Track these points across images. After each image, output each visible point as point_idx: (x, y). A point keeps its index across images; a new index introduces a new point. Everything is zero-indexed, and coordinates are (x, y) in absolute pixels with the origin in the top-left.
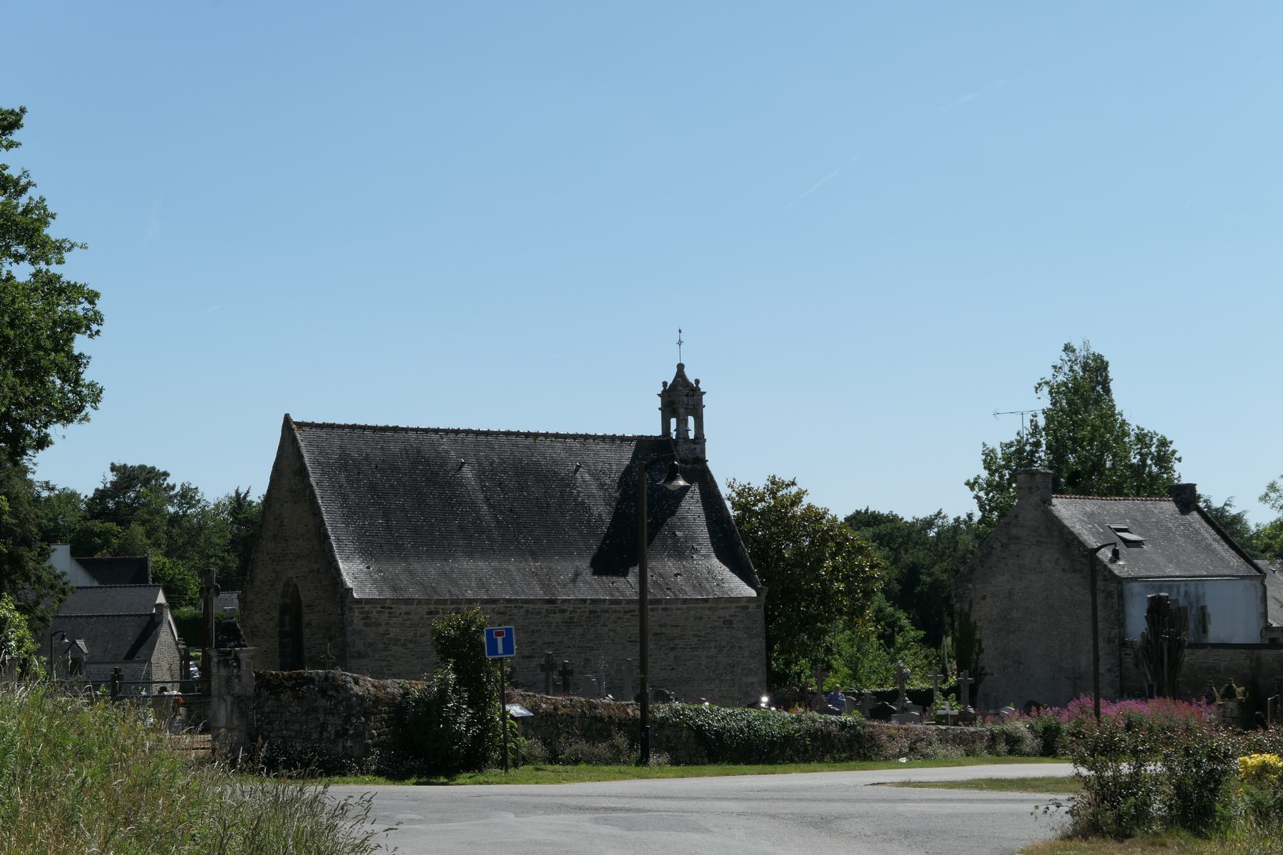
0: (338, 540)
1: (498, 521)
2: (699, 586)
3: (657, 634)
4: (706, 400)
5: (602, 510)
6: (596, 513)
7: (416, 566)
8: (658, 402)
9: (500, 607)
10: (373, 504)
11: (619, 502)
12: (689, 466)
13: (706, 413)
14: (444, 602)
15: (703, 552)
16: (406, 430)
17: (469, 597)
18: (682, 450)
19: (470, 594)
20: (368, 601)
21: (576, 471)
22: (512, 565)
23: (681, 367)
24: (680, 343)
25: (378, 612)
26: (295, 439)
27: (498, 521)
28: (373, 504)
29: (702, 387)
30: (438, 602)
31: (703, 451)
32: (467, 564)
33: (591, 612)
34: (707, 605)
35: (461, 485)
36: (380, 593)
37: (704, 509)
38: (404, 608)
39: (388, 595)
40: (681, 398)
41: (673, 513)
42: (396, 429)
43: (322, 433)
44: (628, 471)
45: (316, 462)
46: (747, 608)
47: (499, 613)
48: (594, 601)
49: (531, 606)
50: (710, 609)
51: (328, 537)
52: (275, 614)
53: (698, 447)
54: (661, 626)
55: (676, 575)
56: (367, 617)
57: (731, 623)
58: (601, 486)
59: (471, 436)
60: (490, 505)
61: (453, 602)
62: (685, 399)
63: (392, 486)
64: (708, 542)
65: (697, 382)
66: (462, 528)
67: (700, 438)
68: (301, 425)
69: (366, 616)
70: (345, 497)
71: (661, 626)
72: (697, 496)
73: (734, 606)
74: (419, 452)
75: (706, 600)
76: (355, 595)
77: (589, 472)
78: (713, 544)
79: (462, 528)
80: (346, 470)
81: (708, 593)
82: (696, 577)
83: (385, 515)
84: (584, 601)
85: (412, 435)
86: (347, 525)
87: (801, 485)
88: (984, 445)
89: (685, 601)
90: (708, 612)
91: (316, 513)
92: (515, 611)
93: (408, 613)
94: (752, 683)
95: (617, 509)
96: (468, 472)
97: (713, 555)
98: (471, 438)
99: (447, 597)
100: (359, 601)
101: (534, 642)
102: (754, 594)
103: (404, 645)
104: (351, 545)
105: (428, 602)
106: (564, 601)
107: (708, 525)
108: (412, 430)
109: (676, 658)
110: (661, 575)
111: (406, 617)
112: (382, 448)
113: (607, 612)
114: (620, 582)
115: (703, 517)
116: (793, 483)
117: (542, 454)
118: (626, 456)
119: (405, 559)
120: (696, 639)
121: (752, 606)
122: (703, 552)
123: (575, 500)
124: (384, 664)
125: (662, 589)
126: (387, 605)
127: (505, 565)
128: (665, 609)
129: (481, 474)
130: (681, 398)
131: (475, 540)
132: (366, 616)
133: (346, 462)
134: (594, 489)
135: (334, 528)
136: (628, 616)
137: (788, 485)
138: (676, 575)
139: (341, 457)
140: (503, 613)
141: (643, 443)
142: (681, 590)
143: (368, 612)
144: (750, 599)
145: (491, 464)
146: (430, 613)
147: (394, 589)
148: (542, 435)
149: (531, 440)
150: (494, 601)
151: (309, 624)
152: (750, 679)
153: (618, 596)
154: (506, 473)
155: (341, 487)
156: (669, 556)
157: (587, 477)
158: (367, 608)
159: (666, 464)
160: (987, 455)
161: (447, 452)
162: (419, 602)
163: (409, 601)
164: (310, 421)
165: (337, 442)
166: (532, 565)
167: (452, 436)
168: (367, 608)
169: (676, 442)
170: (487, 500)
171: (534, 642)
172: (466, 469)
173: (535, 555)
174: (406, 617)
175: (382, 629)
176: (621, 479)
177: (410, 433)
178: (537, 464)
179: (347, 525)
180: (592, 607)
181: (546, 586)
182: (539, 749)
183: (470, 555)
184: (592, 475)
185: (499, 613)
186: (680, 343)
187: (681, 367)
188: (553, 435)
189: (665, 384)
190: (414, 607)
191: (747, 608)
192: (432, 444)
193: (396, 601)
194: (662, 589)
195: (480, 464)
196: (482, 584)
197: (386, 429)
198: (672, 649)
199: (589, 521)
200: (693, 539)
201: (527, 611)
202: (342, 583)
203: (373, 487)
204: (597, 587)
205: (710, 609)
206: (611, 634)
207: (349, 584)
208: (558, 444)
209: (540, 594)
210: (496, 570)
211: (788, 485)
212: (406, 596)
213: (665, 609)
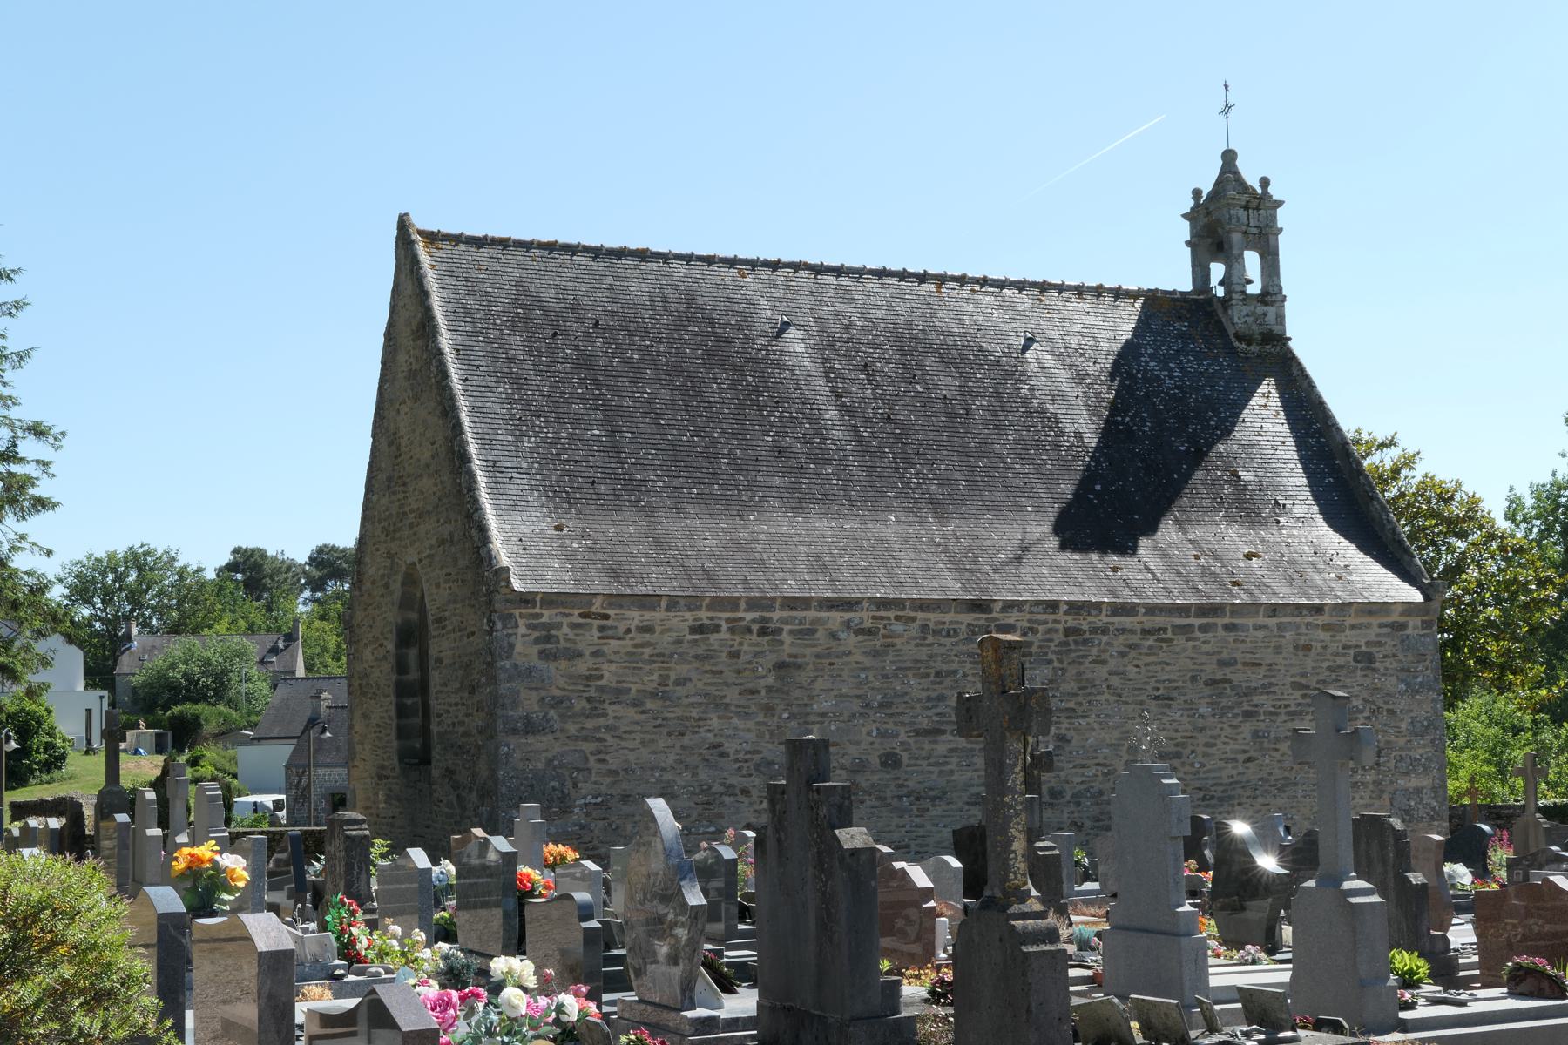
0: (493, 468)
1: (860, 440)
2: (1298, 578)
3: (1212, 683)
4: (1283, 217)
5: (1082, 424)
6: (1069, 429)
7: (670, 525)
8: (1184, 230)
9: (864, 616)
10: (582, 397)
11: (1114, 408)
12: (1254, 348)
13: (1286, 246)
14: (733, 603)
15: (1298, 513)
16: (665, 257)
17: (789, 592)
18: (1239, 317)
19: (791, 588)
20: (550, 600)
21: (1025, 348)
22: (892, 529)
23: (1229, 157)
24: (1227, 109)
25: (574, 626)
26: (415, 261)
27: (860, 440)
28: (582, 397)
29: (1275, 192)
30: (718, 603)
31: (1281, 318)
32: (786, 525)
33: (1069, 632)
34: (1320, 620)
35: (780, 365)
36: (578, 583)
37: (1292, 429)
38: (635, 617)
39: (598, 584)
40: (1232, 217)
41: (1227, 432)
42: (643, 255)
43: (482, 255)
44: (1128, 354)
45: (452, 311)
46: (1403, 626)
47: (860, 631)
48: (1075, 608)
49: (932, 617)
50: (1327, 627)
51: (465, 459)
52: (390, 646)
53: (1271, 310)
54: (1222, 664)
55: (1249, 556)
56: (548, 639)
57: (1370, 658)
58: (1079, 377)
59: (803, 274)
60: (843, 408)
61: (753, 604)
62: (1242, 213)
63: (627, 363)
64: (1306, 492)
65: (1265, 182)
66: (780, 451)
67: (1272, 295)
68: (432, 238)
69: (546, 635)
70: (518, 381)
71: (1222, 664)
72: (1275, 403)
73: (1375, 621)
74: (691, 299)
75: (1318, 609)
76: (517, 585)
77: (1052, 349)
78: (1316, 497)
79: (780, 451)
80: (526, 328)
81: (1322, 594)
82: (1291, 562)
83: (610, 421)
84: (1053, 606)
85: (681, 267)
86: (519, 438)
87: (1407, 444)
88: (1511, 489)
89: (1274, 610)
90: (1323, 635)
91: (457, 427)
92: (898, 628)
93: (648, 629)
94: (1418, 791)
95: (1108, 422)
96: (796, 343)
97: (1319, 518)
98: (804, 278)
99: (739, 592)
100: (526, 599)
101: (941, 698)
102: (1416, 596)
103: (636, 704)
104: (522, 481)
105: (693, 603)
106: (1009, 606)
107: (1302, 459)
108: (679, 257)
109: (1256, 734)
110: (1215, 556)
111: (640, 638)
112: (611, 289)
113: (1104, 631)
114: (1129, 566)
115: (1290, 442)
116: (1392, 443)
117: (956, 315)
118: (1124, 323)
119: (649, 511)
120: (1298, 694)
121: (1414, 622)
122: (1298, 513)
123: (1025, 404)
124: (588, 747)
125: (1222, 585)
126: (596, 608)
127: (874, 528)
128: (1230, 628)
129: (824, 347)
130: (1232, 217)
131: (808, 474)
132: (546, 635)
133: (528, 313)
134: (1065, 384)
135: (486, 444)
136: (1151, 641)
137: (1383, 446)
138: (1249, 556)
139: (517, 303)
140: (870, 632)
141: (1156, 305)
142: (1263, 587)
143: (548, 627)
144: (1409, 608)
145: (847, 328)
146: (699, 629)
147: (615, 574)
148: (953, 279)
149: (930, 287)
150: (849, 604)
151: (439, 661)
152: (1414, 782)
153: (1126, 596)
154: (877, 346)
155: (511, 360)
156: (1229, 518)
157: (1049, 361)
158: (547, 615)
159: (1200, 367)
160: (1512, 502)
161: (752, 302)
162: (673, 603)
163: (647, 601)
164: (454, 230)
165: (512, 273)
166: (935, 530)
167: (765, 273)
168: (547, 615)
169: (1225, 302)
170: (837, 396)
171: (941, 698)
172: (791, 334)
173: (940, 510)
174: (640, 638)
175: (582, 667)
176: (1116, 364)
177: (675, 264)
178: (944, 331)
179: (519, 438)
180: (1071, 621)
181: (967, 574)
182: (931, 364)
183: (797, 505)
184: (1060, 357)
185: (860, 631)
186: (1227, 109)
187: (1229, 157)
188: (976, 281)
189: (1197, 193)
190: (659, 615)
191: (1403, 626)
192: (720, 285)
193: (614, 600)
194: (1222, 585)
195: (823, 328)
196: (821, 567)
197: (621, 253)
198: (1248, 715)
199: (1057, 446)
200: (1277, 486)
201: (925, 627)
202: (490, 558)
203: (584, 364)
204: (1081, 577)
205: (1327, 627)
206: (1115, 681)
207: (505, 560)
208: (987, 298)
209: (955, 589)
210: (854, 538)
211: (1383, 446)
212: (641, 589)
213: (1230, 628)
